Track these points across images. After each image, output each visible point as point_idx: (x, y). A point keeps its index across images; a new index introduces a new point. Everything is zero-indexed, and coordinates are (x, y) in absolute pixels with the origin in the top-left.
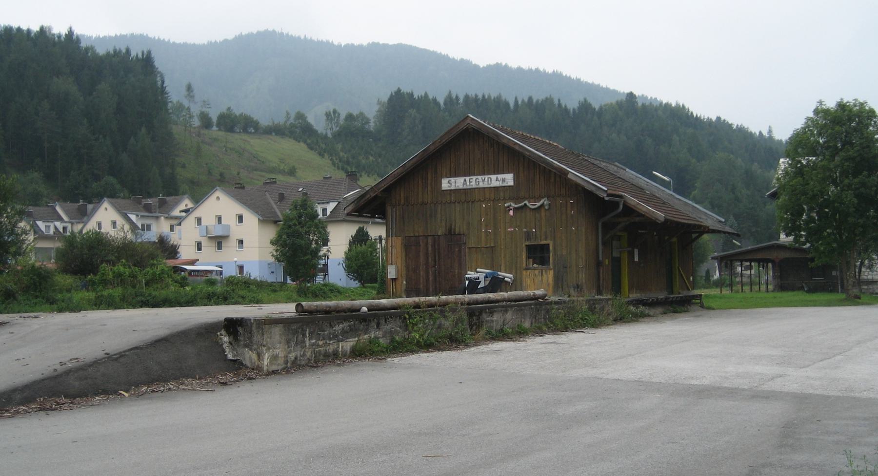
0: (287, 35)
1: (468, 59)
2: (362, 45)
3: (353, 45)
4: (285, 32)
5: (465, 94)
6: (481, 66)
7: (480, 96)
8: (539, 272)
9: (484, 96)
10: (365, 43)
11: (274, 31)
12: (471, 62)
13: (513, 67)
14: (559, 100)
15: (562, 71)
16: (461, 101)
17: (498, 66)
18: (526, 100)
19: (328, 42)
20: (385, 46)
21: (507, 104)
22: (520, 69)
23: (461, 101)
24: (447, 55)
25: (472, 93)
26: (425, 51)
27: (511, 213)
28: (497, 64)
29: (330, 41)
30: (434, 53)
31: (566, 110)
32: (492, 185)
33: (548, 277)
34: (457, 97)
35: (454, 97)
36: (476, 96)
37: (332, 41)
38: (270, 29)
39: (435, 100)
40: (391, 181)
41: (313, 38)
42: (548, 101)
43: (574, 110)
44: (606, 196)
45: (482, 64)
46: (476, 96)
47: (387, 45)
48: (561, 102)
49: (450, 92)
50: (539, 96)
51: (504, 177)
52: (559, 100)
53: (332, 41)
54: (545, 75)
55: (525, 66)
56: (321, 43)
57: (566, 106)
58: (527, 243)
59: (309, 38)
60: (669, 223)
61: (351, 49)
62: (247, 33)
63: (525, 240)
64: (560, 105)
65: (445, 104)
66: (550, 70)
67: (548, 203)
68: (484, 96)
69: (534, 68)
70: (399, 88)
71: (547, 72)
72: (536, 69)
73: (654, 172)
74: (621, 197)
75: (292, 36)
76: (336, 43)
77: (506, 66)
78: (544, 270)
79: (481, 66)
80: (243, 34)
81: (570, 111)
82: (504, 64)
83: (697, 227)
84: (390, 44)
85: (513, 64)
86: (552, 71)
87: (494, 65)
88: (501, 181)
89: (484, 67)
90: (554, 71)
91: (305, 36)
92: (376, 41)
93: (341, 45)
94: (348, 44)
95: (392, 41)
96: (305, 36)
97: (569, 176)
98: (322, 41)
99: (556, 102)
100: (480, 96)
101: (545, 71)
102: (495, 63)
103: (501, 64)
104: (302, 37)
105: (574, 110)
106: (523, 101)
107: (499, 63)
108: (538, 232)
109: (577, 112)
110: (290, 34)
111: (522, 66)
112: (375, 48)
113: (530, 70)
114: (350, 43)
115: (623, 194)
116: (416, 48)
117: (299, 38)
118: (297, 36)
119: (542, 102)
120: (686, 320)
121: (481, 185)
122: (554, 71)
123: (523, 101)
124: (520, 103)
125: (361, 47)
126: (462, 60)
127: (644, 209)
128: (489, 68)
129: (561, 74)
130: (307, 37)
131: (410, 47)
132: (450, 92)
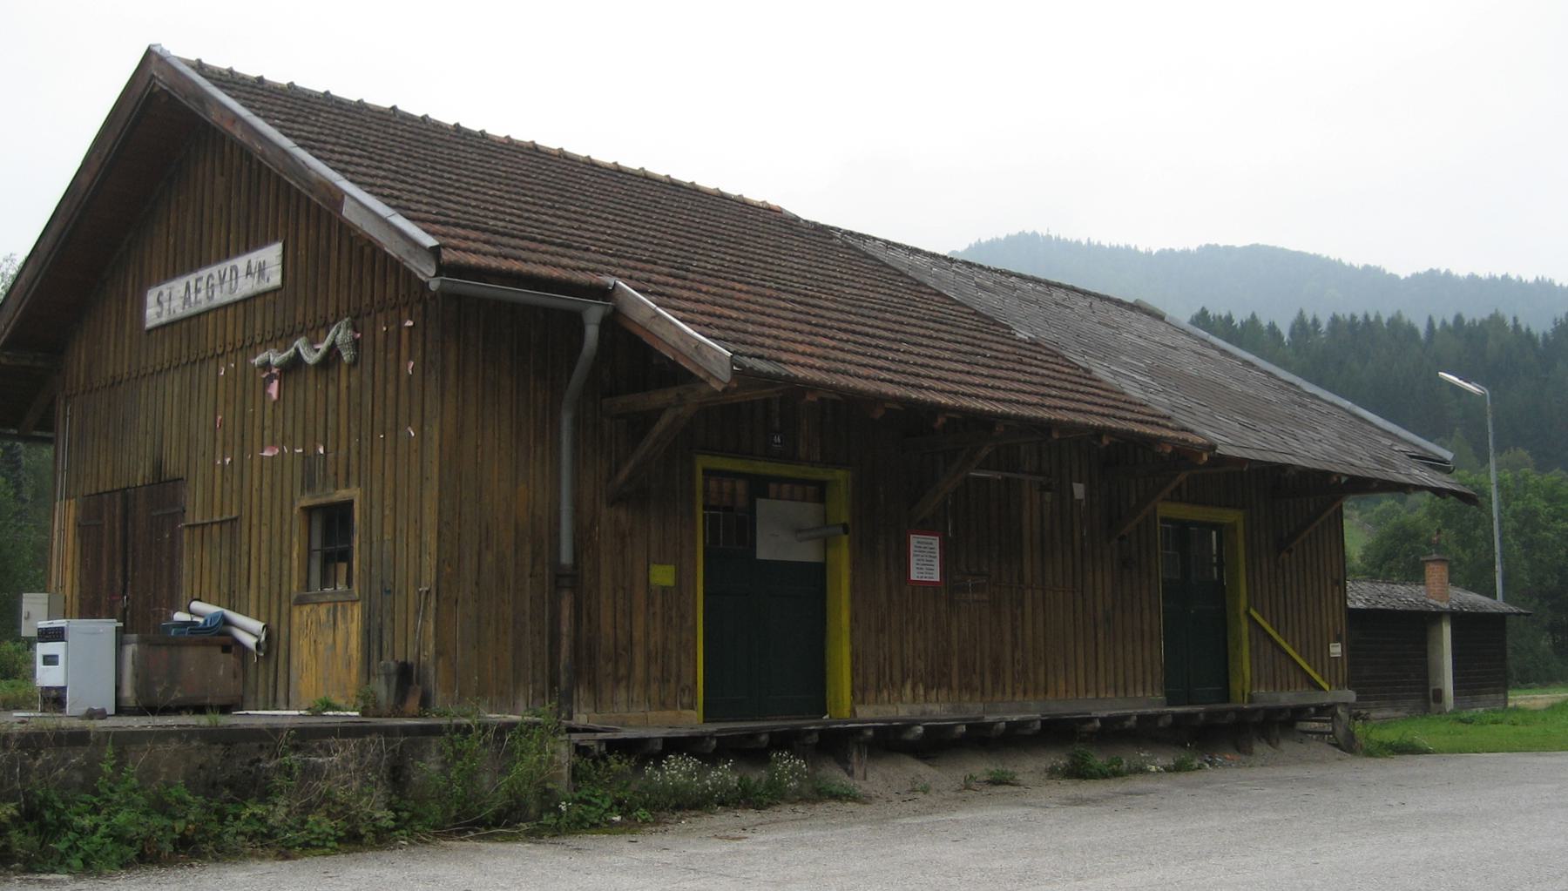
0: (1058, 239)
1: (1378, 265)
2: (1189, 250)
3: (1172, 250)
4: (1054, 234)
5: (1331, 315)
6: (1402, 277)
7: (1360, 318)
8: (328, 611)
9: (1366, 317)
10: (1193, 247)
11: (1035, 234)
12: (1384, 271)
13: (1460, 275)
14: (1515, 319)
15: (1552, 278)
16: (1324, 327)
17: (1432, 274)
18: (1450, 321)
19: (1128, 248)
20: (1229, 250)
21: (1412, 331)
22: (1473, 279)
23: (1324, 327)
24: (1340, 260)
25: (1345, 312)
26: (1299, 257)
27: (274, 390)
28: (1431, 270)
29: (1133, 247)
30: (1316, 258)
31: (1529, 335)
32: (238, 295)
33: (348, 633)
34: (1315, 321)
35: (1310, 322)
36: (1353, 317)
37: (1136, 247)
38: (1029, 231)
39: (1272, 327)
40: (17, 310)
41: (1103, 243)
42: (1496, 320)
43: (1545, 334)
44: (432, 272)
45: (1404, 272)
46: (1353, 317)
47: (1233, 247)
48: (1519, 322)
49: (1301, 313)
50: (1475, 313)
51: (262, 260)
52: (1515, 319)
53: (1136, 247)
54: (1521, 286)
55: (1483, 273)
56: (1115, 252)
57: (1528, 329)
58: (307, 501)
59: (1096, 243)
60: (941, 420)
61: (1167, 256)
62: (989, 239)
63: (302, 491)
64: (1516, 327)
65: (1292, 334)
66: (1529, 277)
67: (348, 339)
68: (1366, 317)
69: (1499, 276)
70: (1203, 308)
71: (1524, 280)
72: (1503, 277)
73: (1442, 374)
74: (604, 293)
75: (1066, 240)
76: (1142, 249)
77: (1448, 273)
78: (339, 605)
79: (1402, 277)
80: (983, 241)
81: (1537, 338)
82: (1443, 271)
83: (1375, 485)
84: (1238, 246)
85: (1461, 270)
86: (1534, 278)
87: (1425, 273)
88: (256, 275)
89: (1406, 278)
90: (1537, 278)
91: (1089, 239)
92: (1213, 243)
93: (1151, 253)
94: (1164, 250)
95: (1240, 241)
96: (1089, 239)
97: (348, 212)
98: (1118, 246)
99: (1510, 322)
100: (1360, 318)
101: (1521, 280)
102: (1427, 269)
103: (1438, 271)
104: (1084, 242)
105: (1545, 334)
106: (1444, 323)
107: (1435, 268)
108: (331, 456)
109: (1551, 338)
110: (1062, 238)
111: (1476, 273)
112: (1210, 251)
113: (1493, 279)
114: (1167, 248)
115: (611, 281)
116: (1283, 250)
117: (1078, 243)
118: (1074, 240)
119: (1481, 324)
120: (40, 880)
121: (220, 297)
122: (1537, 278)
123: (1444, 323)
124: (1437, 326)
125: (1185, 254)
126: (1367, 268)
127: (672, 338)
128: (1416, 278)
129: (1551, 283)
130: (1092, 240)
131: (1273, 249)
132: (1301, 313)
